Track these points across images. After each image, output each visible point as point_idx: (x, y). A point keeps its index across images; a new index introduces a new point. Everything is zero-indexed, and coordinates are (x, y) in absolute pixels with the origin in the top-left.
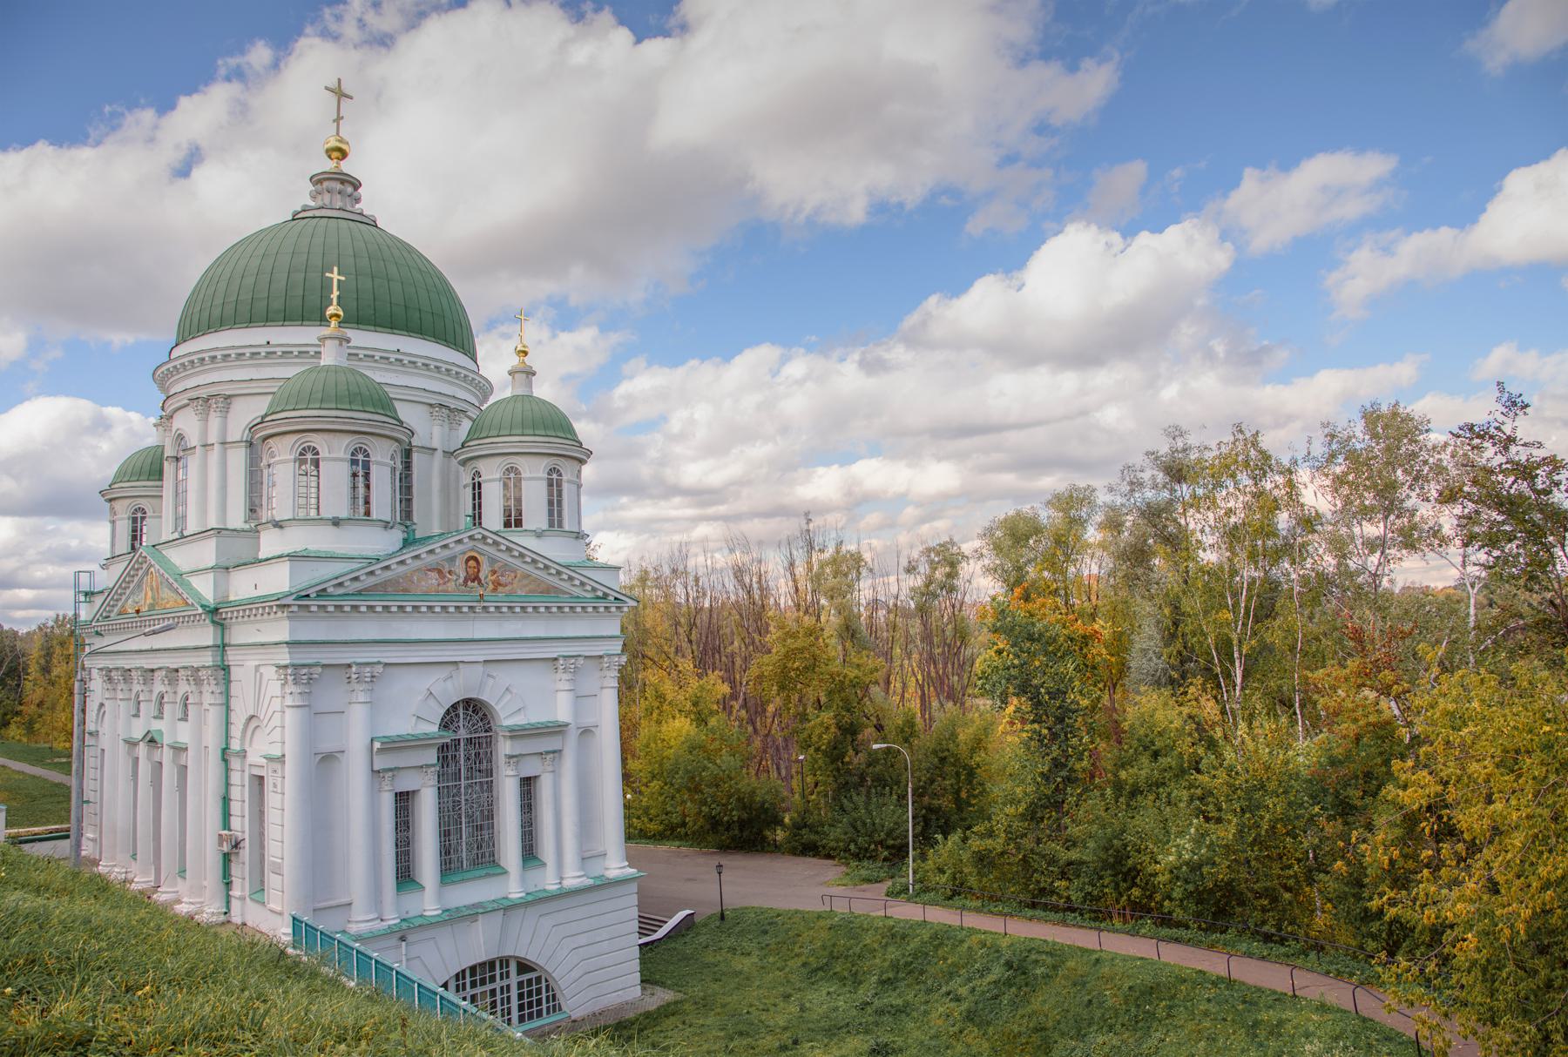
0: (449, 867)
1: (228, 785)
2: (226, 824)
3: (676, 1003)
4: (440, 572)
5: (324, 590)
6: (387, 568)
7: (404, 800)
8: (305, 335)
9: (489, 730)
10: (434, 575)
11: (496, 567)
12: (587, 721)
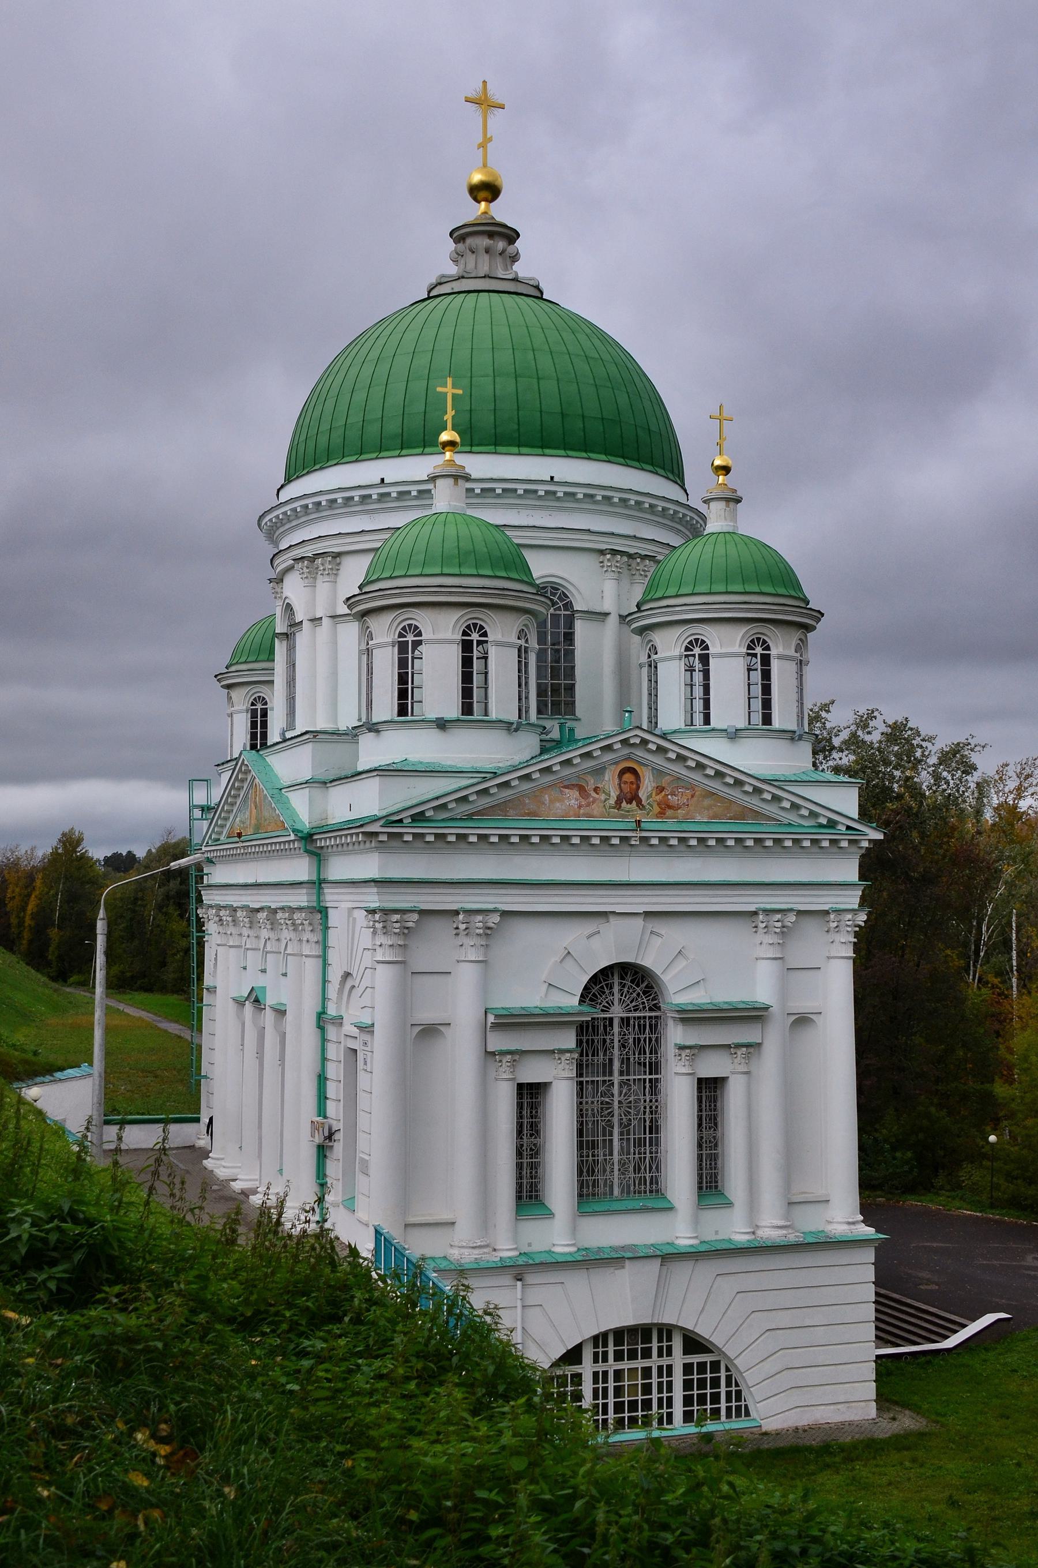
0: (590, 1189)
1: (324, 1059)
2: (322, 1111)
3: (921, 1435)
4: (582, 789)
5: (422, 813)
6: (506, 784)
7: (531, 1096)
8: (413, 468)
9: (656, 1007)
10: (575, 793)
11: (665, 781)
12: (802, 1005)
